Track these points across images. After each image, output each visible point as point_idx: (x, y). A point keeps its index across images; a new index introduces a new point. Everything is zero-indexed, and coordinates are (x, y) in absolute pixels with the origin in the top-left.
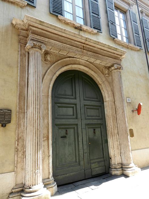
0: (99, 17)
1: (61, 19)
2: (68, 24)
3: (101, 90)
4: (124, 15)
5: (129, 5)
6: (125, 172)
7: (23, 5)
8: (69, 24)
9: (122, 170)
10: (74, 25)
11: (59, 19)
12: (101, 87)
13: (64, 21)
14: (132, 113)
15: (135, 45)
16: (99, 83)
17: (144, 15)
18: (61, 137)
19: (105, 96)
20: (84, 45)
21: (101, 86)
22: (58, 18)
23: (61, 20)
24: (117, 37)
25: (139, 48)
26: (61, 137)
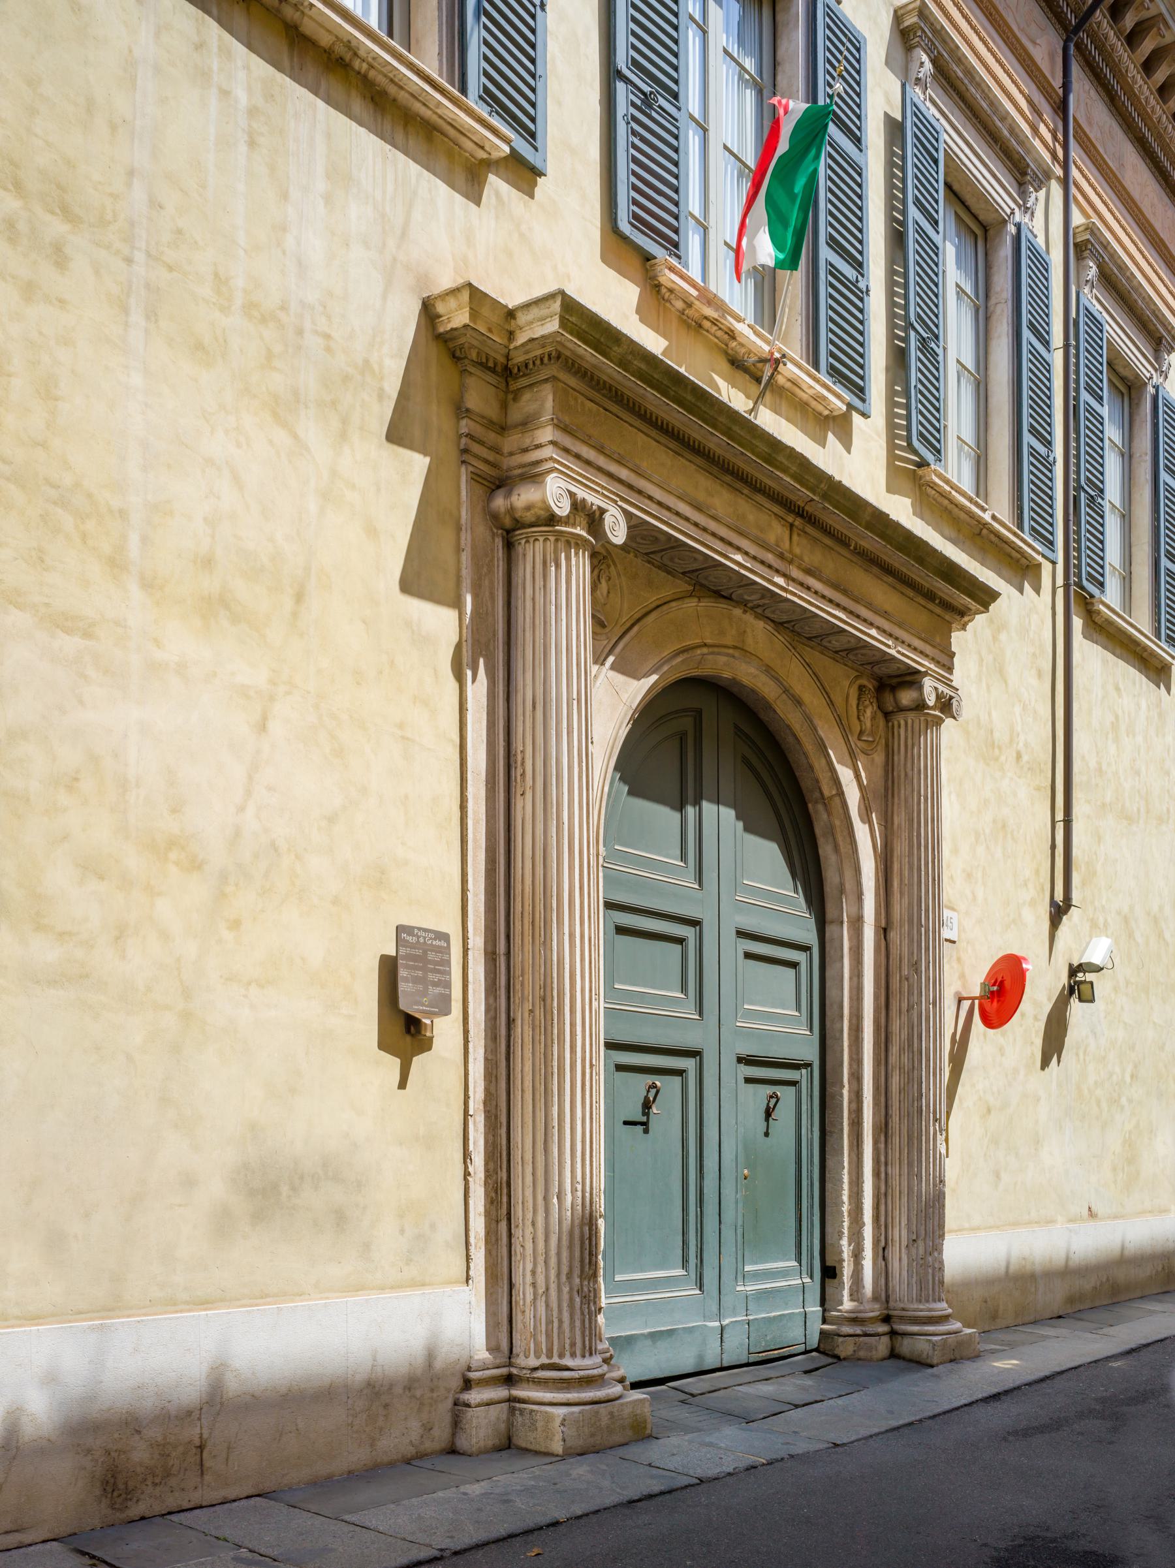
0: (862, 285)
1: (670, 285)
2: (700, 326)
3: (821, 841)
4: (970, 242)
5: (1024, 174)
6: (906, 1346)
7: (482, 155)
8: (707, 324)
9: (893, 1333)
10: (733, 338)
11: (658, 286)
12: (825, 816)
13: (679, 305)
14: (408, 1038)
15: (816, 366)
16: (822, 794)
17: (1092, 271)
18: (626, 1123)
19: (842, 884)
20: (797, 523)
21: (829, 814)
22: (654, 278)
23: (671, 291)
24: (674, 247)
25: (837, 400)
26: (626, 1123)
